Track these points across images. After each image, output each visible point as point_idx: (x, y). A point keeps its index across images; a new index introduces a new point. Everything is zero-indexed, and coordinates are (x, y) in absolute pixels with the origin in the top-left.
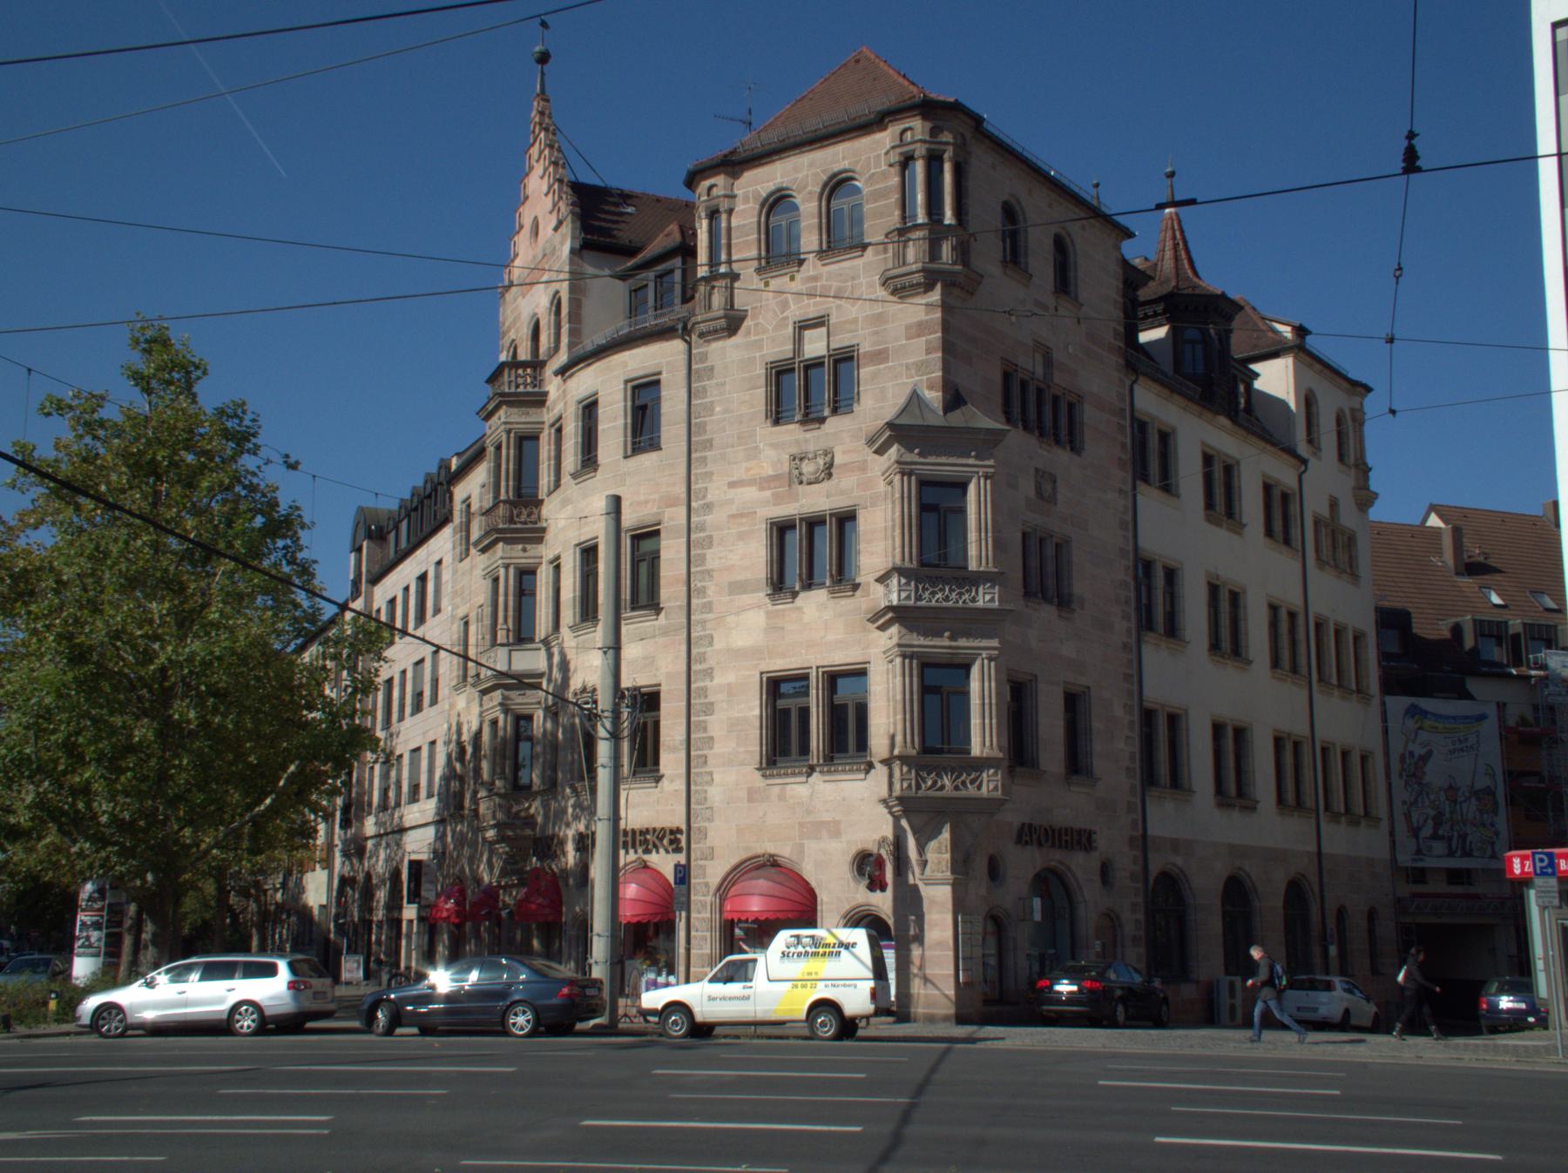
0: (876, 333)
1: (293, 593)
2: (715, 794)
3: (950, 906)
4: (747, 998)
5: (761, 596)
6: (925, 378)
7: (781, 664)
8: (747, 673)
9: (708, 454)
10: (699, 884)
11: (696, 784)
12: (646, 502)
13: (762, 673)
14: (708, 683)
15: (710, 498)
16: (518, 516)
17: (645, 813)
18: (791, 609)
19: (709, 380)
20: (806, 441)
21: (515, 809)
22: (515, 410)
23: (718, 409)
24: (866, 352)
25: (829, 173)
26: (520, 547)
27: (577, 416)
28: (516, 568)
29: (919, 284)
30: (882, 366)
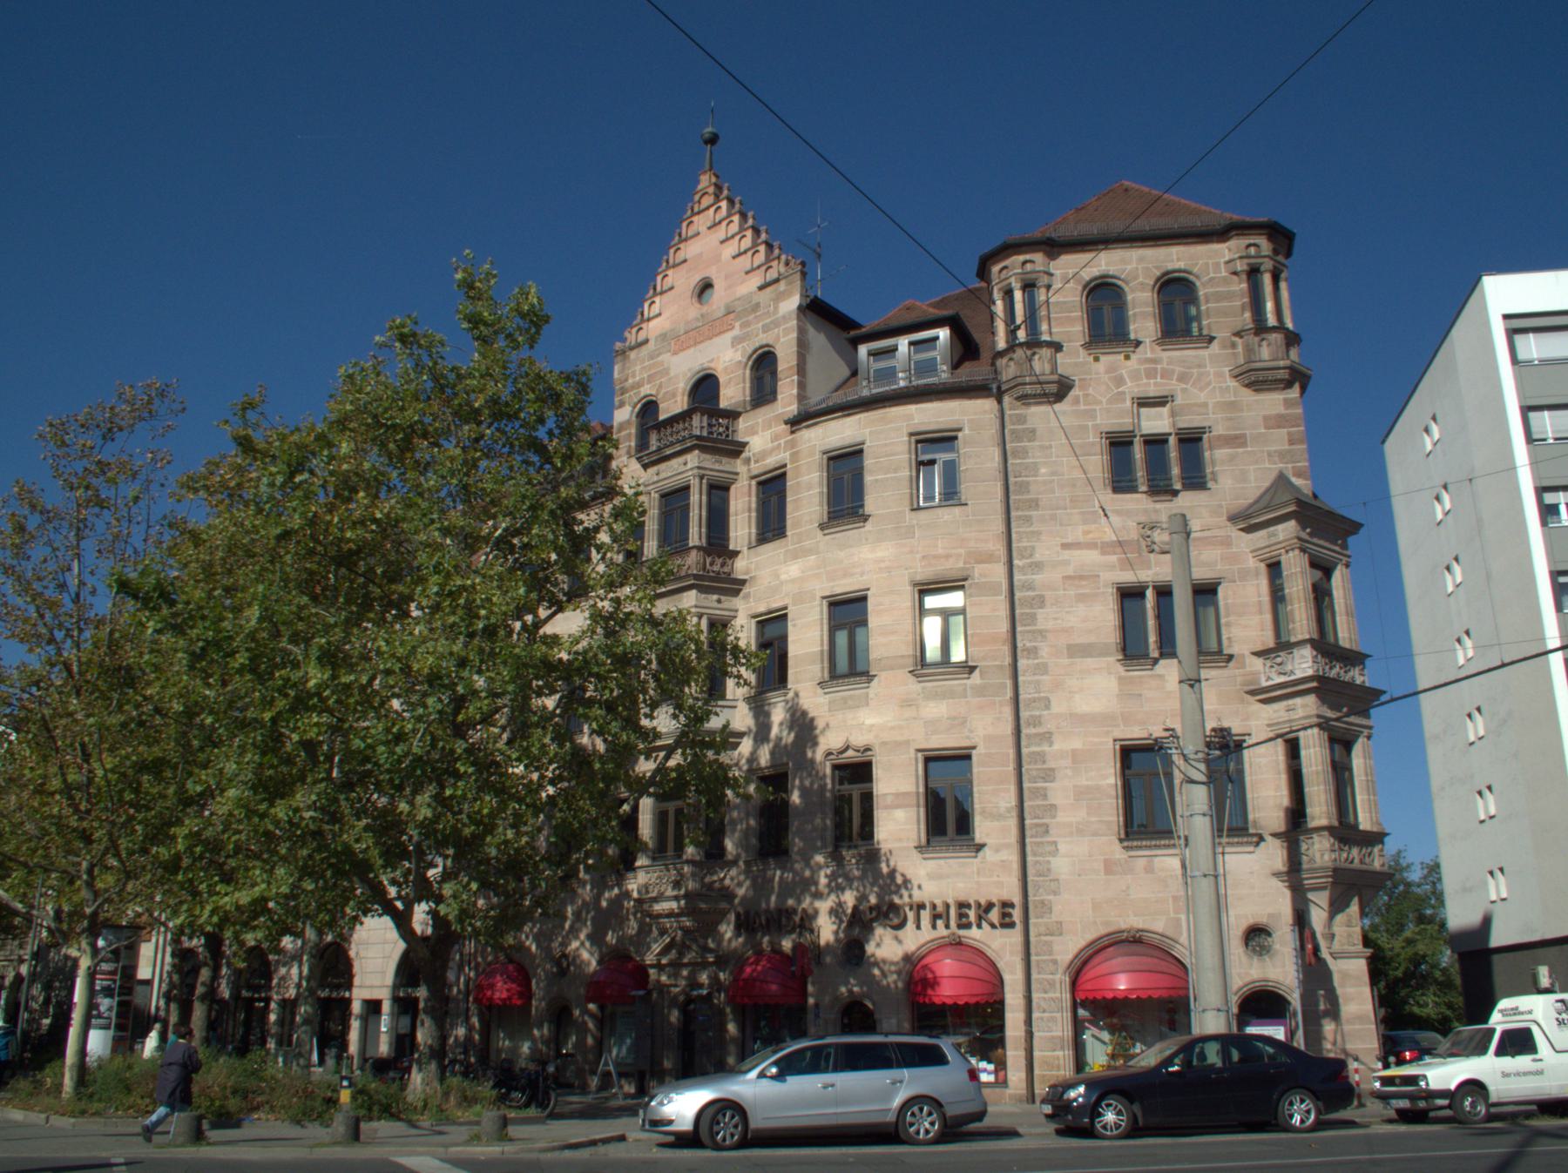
0: (1230, 419)
1: (550, 608)
2: (1061, 865)
3: (1366, 979)
4: (1540, 1073)
5: (1112, 660)
6: (1290, 466)
7: (1135, 733)
8: (1096, 740)
9: (1034, 513)
10: (1044, 961)
11: (1035, 854)
12: (948, 557)
13: (1115, 740)
14: (1046, 748)
15: (1037, 557)
16: (711, 564)
17: (961, 885)
18: (1151, 676)
19: (1029, 441)
20: (1156, 511)
21: (707, 880)
22: (708, 456)
23: (1043, 470)
24: (1220, 436)
25: (1162, 271)
26: (715, 597)
27: (821, 465)
28: (709, 619)
29: (1281, 381)
30: (1240, 450)
